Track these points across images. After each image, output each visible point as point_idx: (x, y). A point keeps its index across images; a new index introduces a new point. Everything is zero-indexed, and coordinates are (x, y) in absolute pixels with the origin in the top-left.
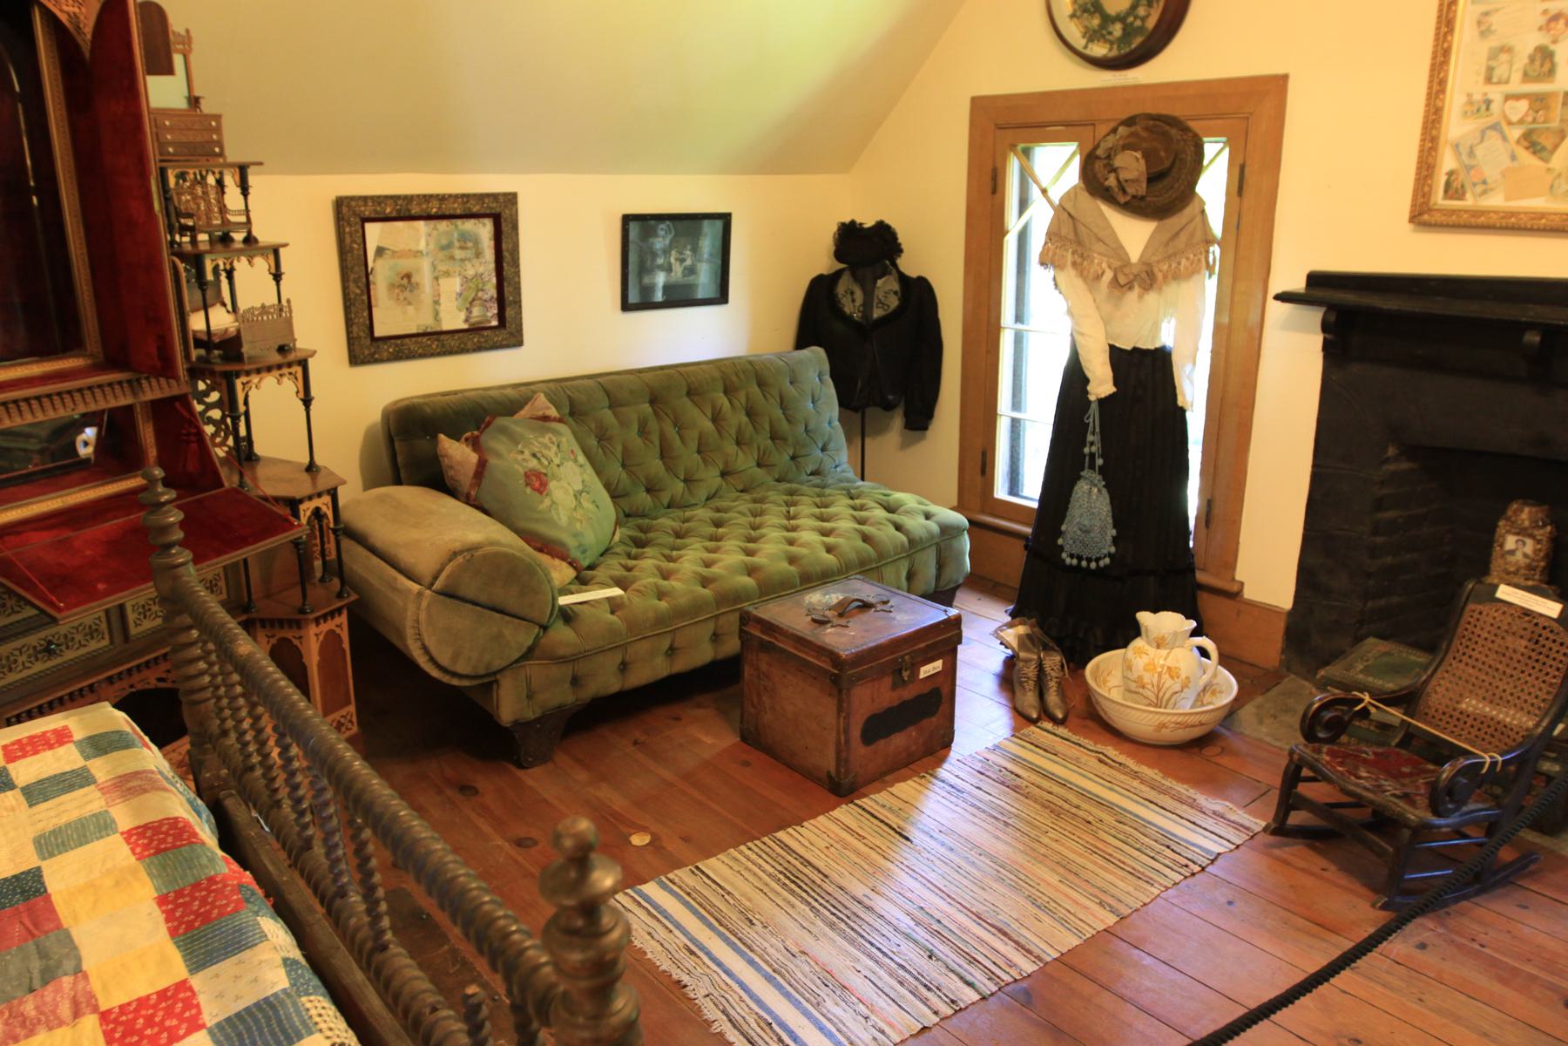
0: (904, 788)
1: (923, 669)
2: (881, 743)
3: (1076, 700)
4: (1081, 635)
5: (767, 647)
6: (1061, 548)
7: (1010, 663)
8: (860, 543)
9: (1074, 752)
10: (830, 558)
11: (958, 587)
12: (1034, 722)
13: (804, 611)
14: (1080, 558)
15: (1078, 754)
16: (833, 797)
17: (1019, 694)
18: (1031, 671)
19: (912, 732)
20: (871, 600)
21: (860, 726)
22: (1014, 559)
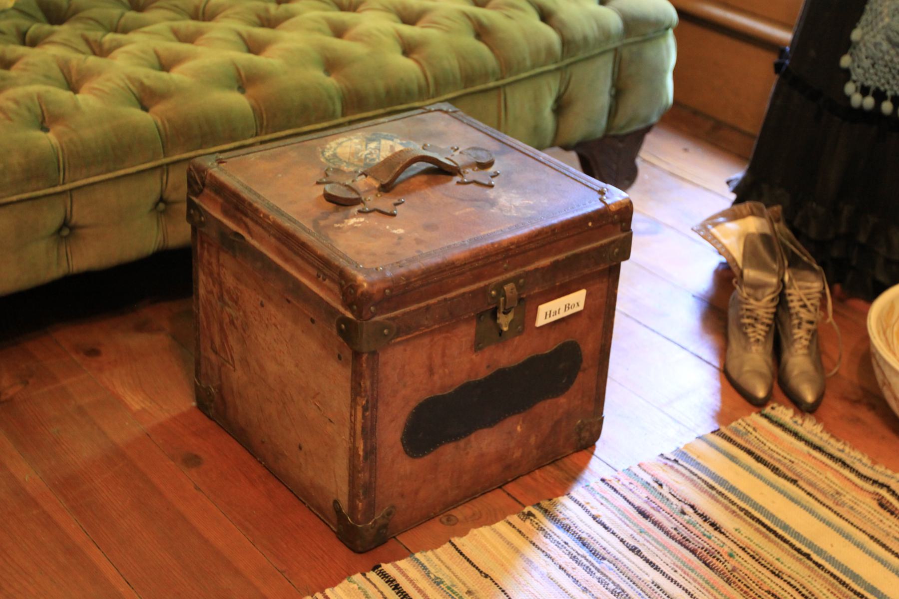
0: (484, 541)
1: (543, 309)
2: (448, 452)
3: (843, 367)
4: (862, 239)
5: (232, 244)
6: (847, 74)
7: (726, 277)
8: (469, 42)
9: (830, 477)
10: (407, 67)
11: (648, 129)
12: (759, 405)
13: (315, 174)
14: (880, 96)
15: (838, 483)
16: (342, 551)
17: (735, 345)
18: (763, 306)
19: (517, 425)
20: (457, 159)
21: (402, 420)
22: (753, 88)
